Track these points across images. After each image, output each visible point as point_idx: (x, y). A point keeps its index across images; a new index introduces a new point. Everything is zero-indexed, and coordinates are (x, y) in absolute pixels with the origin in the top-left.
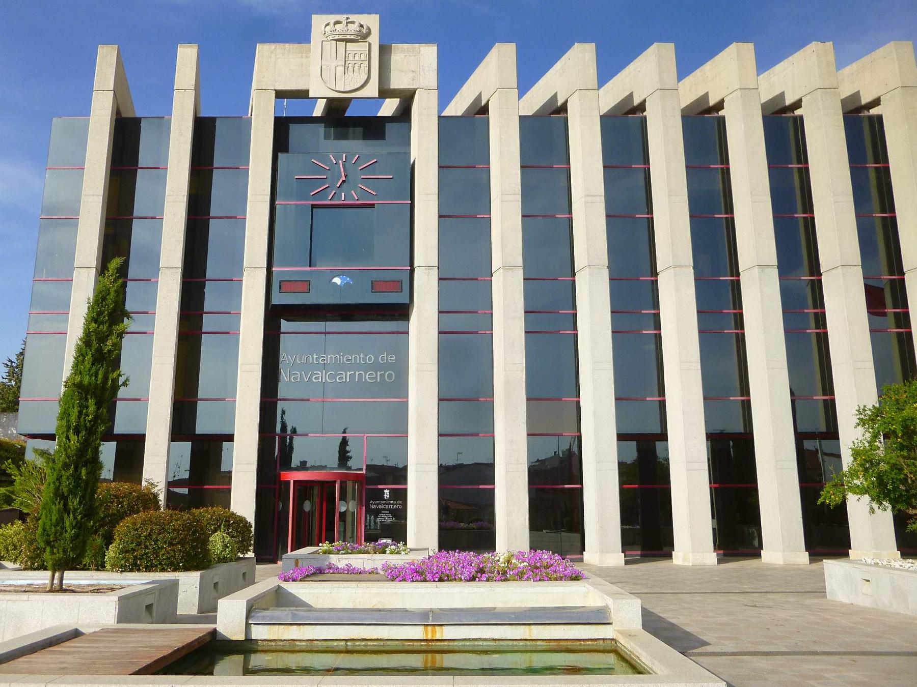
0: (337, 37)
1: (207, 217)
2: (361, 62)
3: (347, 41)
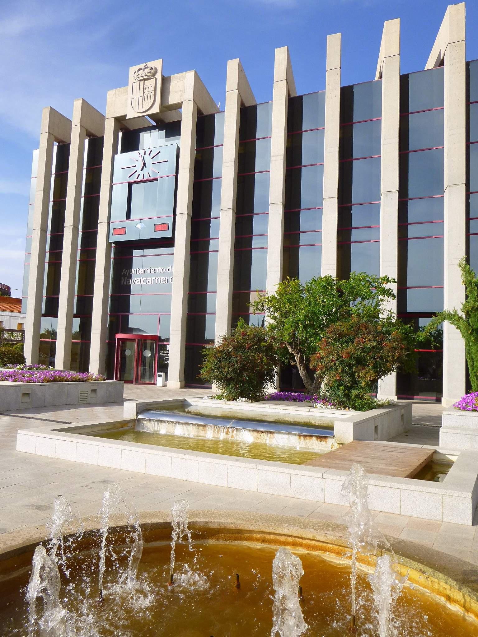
0: (139, 79)
1: (254, 173)
2: (151, 92)
3: (144, 80)
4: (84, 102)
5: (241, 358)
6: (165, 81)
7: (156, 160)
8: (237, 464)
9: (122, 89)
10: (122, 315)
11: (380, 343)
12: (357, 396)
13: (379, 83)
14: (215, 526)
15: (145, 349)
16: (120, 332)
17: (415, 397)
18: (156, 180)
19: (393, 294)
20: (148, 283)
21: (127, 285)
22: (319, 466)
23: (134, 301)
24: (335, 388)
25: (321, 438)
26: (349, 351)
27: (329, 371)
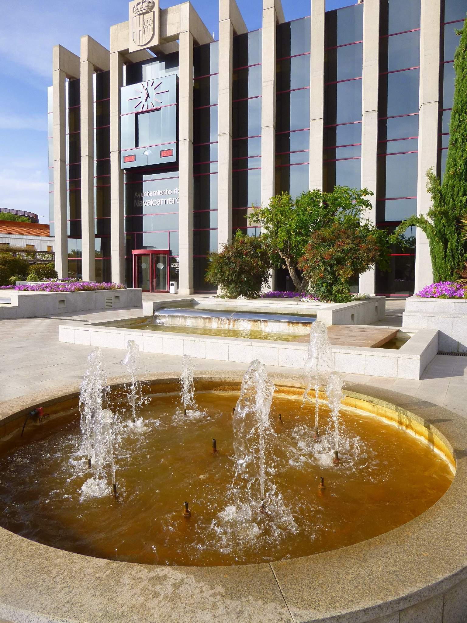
0: (139, 13)
4: (90, 39)
5: (239, 263)
6: (163, 14)
7: (159, 90)
8: (235, 342)
9: (123, 24)
10: (137, 234)
11: (357, 245)
12: (338, 291)
13: (361, 6)
14: (218, 380)
15: (159, 262)
16: (136, 248)
17: (391, 295)
18: (159, 109)
19: (371, 205)
20: (157, 204)
21: (139, 207)
22: (302, 342)
23: (146, 222)
24: (319, 285)
25: (306, 324)
26: (330, 253)
27: (314, 271)
